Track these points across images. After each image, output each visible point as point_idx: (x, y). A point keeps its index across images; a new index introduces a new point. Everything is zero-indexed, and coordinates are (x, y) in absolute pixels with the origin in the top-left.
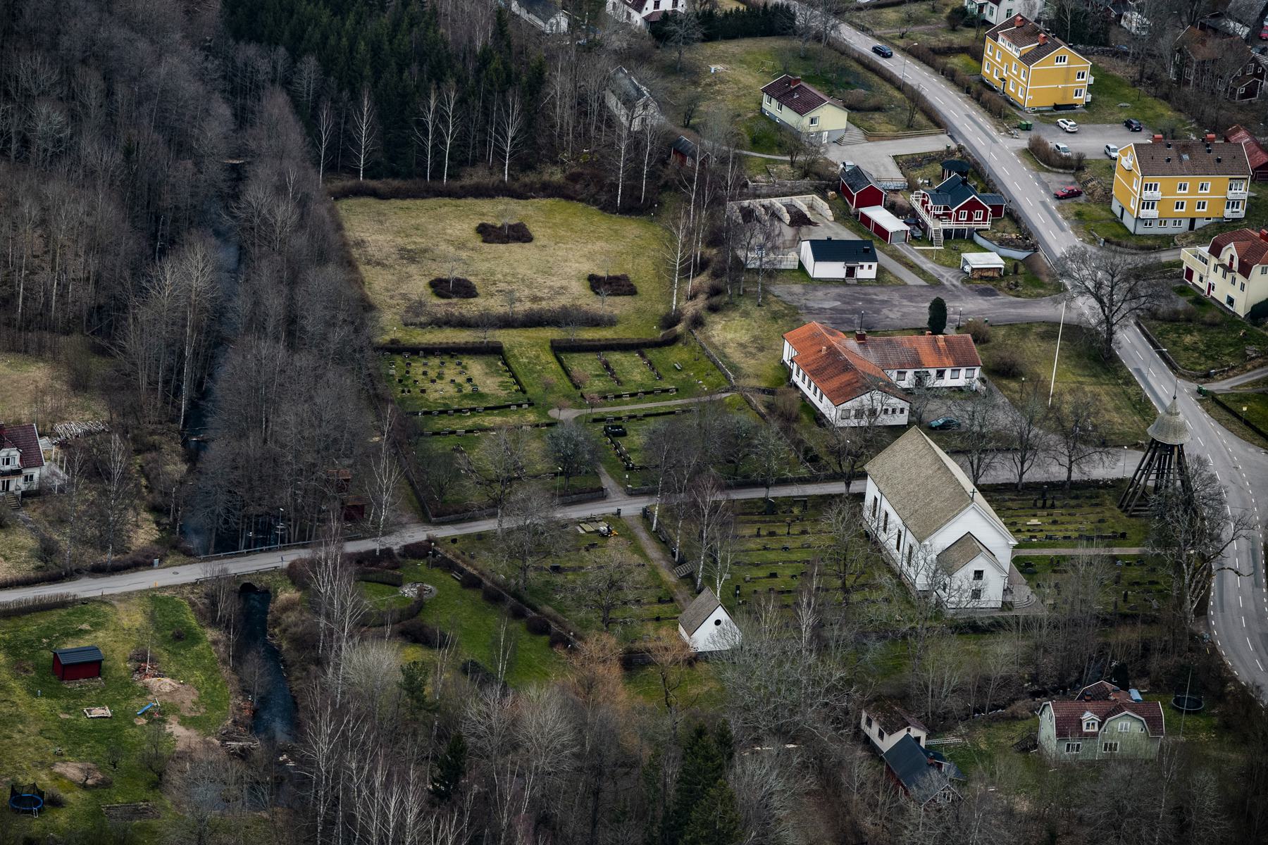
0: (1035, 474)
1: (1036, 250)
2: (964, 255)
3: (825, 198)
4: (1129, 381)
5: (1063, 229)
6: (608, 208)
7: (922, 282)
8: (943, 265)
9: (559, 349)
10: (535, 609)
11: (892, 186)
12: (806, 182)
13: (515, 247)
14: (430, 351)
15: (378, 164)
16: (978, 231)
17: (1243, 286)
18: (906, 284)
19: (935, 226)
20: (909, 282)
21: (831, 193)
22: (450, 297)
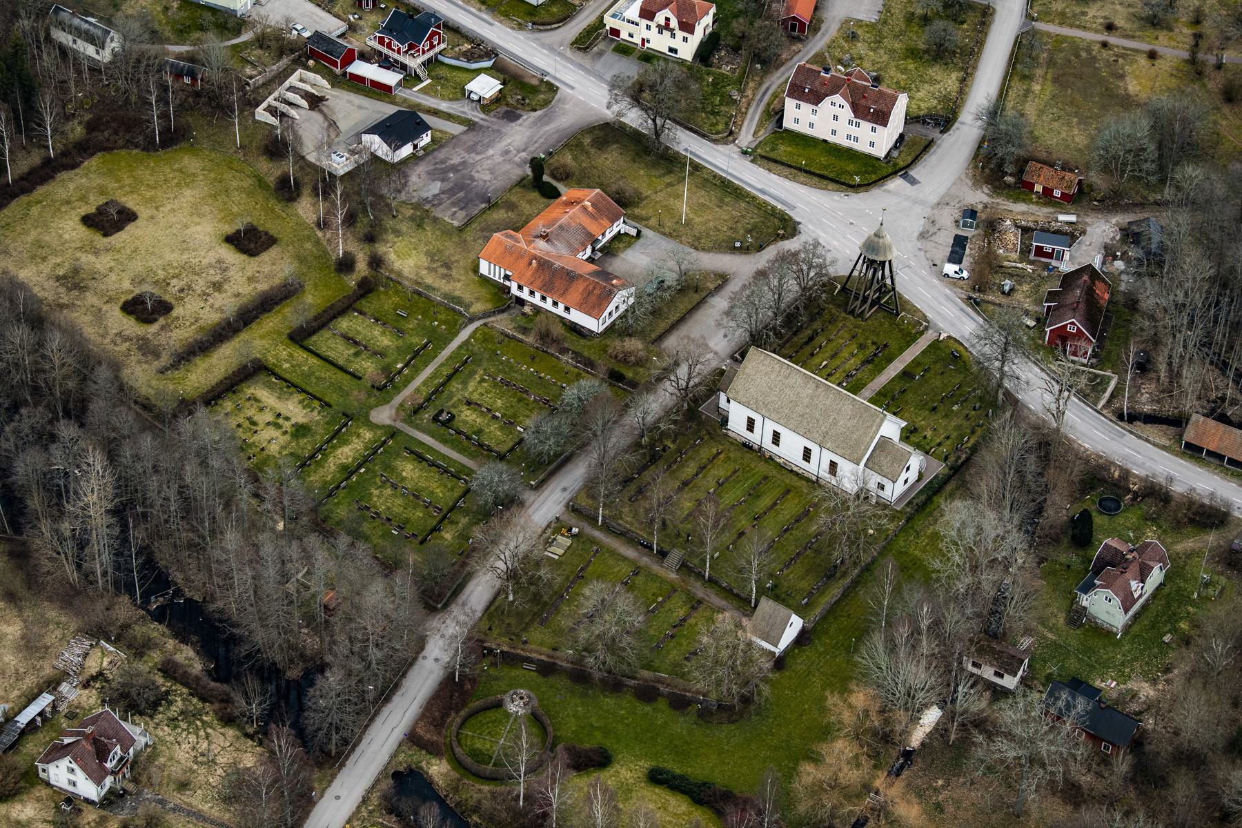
0: (269, 75)
1: (497, 55)
4: (696, 168)
5: (491, 24)
6: (150, 146)
7: (462, 128)
8: (1131, 418)
9: (299, 337)
10: (634, 678)
11: (339, 32)
12: (285, 61)
13: (130, 228)
14: (213, 397)
15: (143, 302)
16: (440, 53)
17: (685, 39)
18: (454, 137)
19: (414, 63)
20: (456, 133)
21: (311, 62)
22: (156, 320)
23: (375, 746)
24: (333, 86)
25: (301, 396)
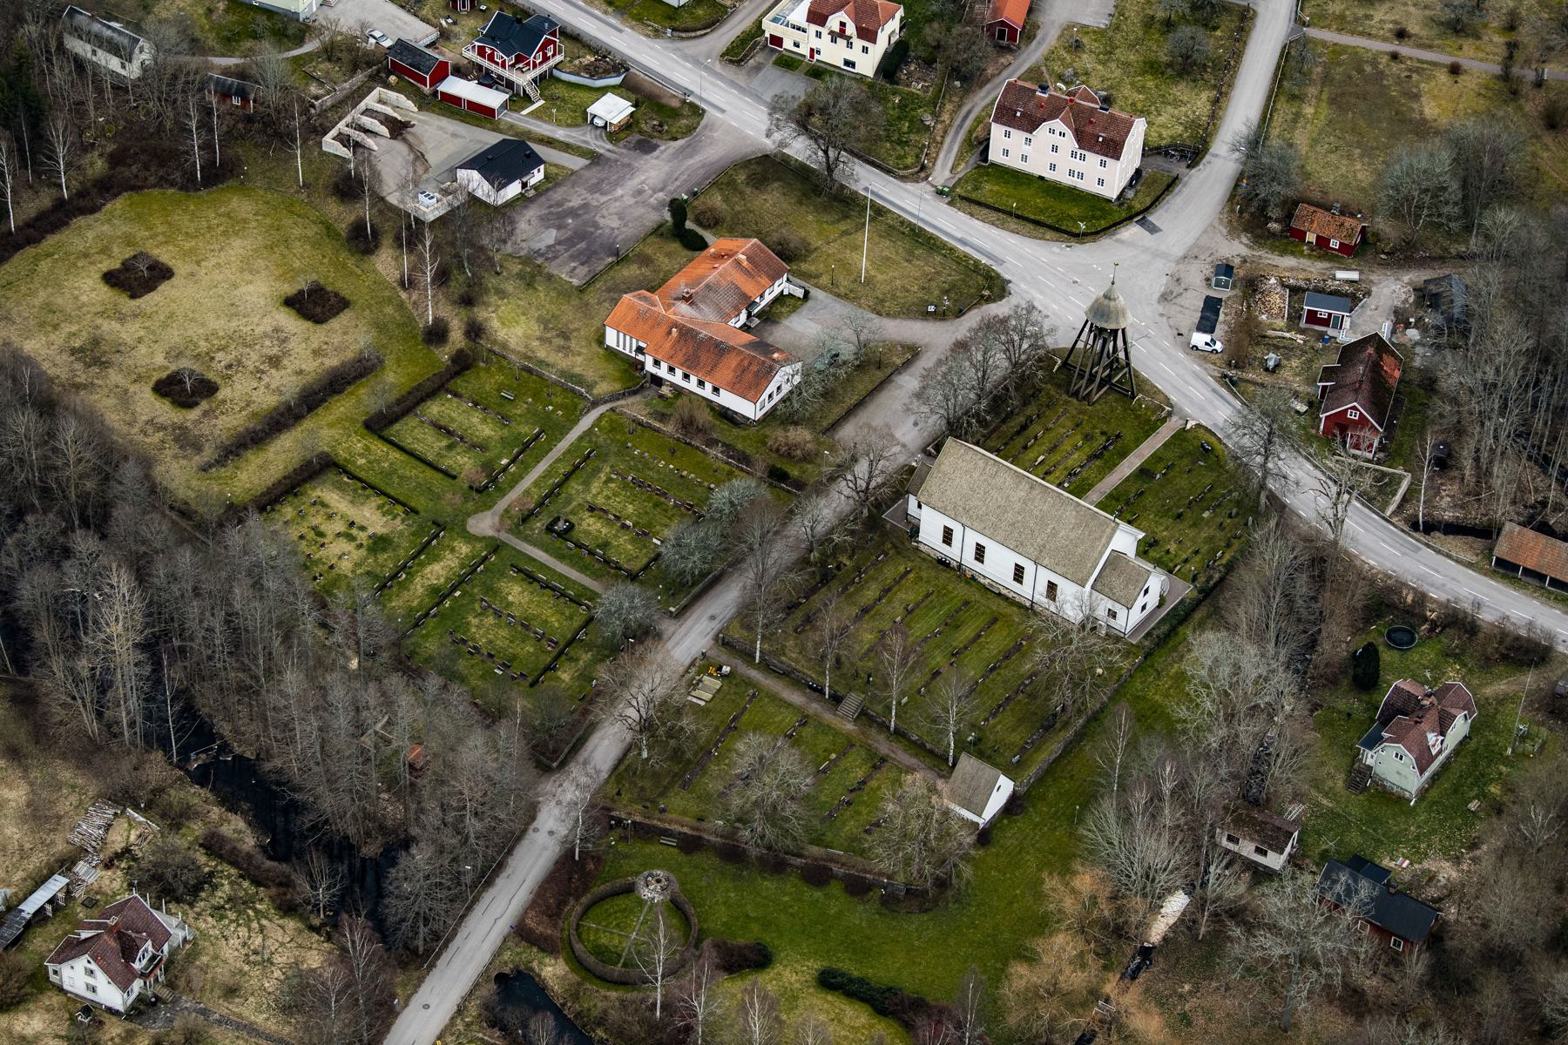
0: (339, 95)
1: (627, 70)
2: (592, 110)
3: (388, 86)
4: (879, 211)
5: (620, 31)
6: (189, 185)
7: (583, 162)
8: (1428, 527)
9: (378, 425)
11: (428, 41)
12: (360, 77)
13: (164, 287)
14: (269, 501)
15: (181, 382)
16: (556, 67)
17: (865, 50)
18: (573, 173)
19: (523, 79)
21: (393, 79)
23: (473, 942)
24: (420, 108)
25: (380, 500)
